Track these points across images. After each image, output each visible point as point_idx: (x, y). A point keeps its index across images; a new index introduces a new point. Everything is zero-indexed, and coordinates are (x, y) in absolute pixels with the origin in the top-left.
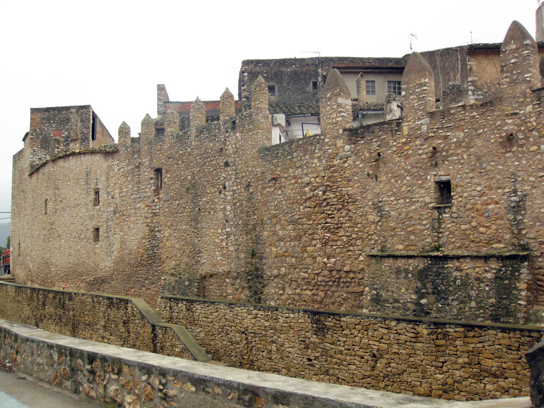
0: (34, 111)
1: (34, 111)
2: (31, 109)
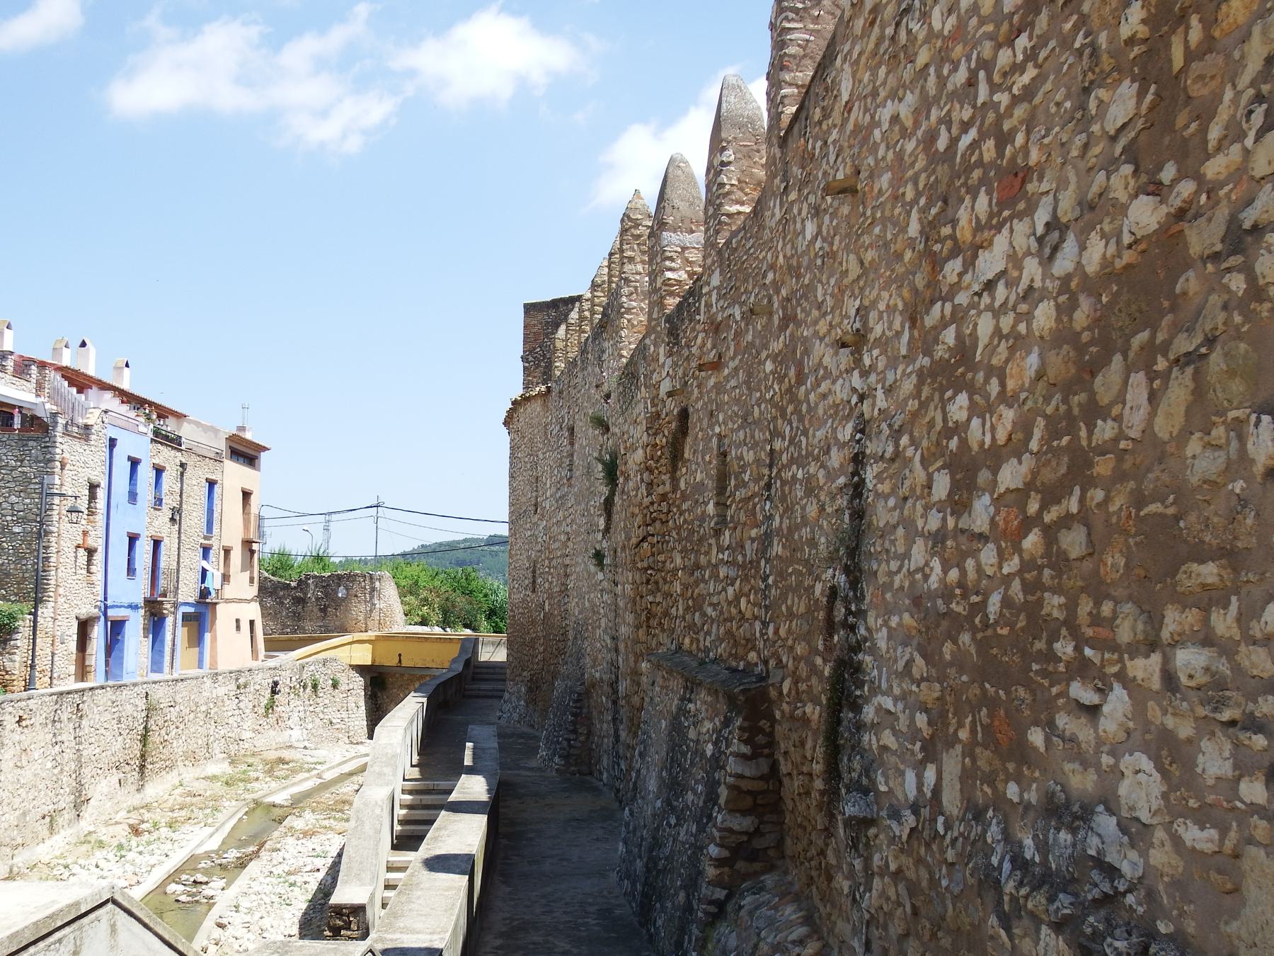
0: (530, 309)
1: (530, 309)
2: (526, 306)
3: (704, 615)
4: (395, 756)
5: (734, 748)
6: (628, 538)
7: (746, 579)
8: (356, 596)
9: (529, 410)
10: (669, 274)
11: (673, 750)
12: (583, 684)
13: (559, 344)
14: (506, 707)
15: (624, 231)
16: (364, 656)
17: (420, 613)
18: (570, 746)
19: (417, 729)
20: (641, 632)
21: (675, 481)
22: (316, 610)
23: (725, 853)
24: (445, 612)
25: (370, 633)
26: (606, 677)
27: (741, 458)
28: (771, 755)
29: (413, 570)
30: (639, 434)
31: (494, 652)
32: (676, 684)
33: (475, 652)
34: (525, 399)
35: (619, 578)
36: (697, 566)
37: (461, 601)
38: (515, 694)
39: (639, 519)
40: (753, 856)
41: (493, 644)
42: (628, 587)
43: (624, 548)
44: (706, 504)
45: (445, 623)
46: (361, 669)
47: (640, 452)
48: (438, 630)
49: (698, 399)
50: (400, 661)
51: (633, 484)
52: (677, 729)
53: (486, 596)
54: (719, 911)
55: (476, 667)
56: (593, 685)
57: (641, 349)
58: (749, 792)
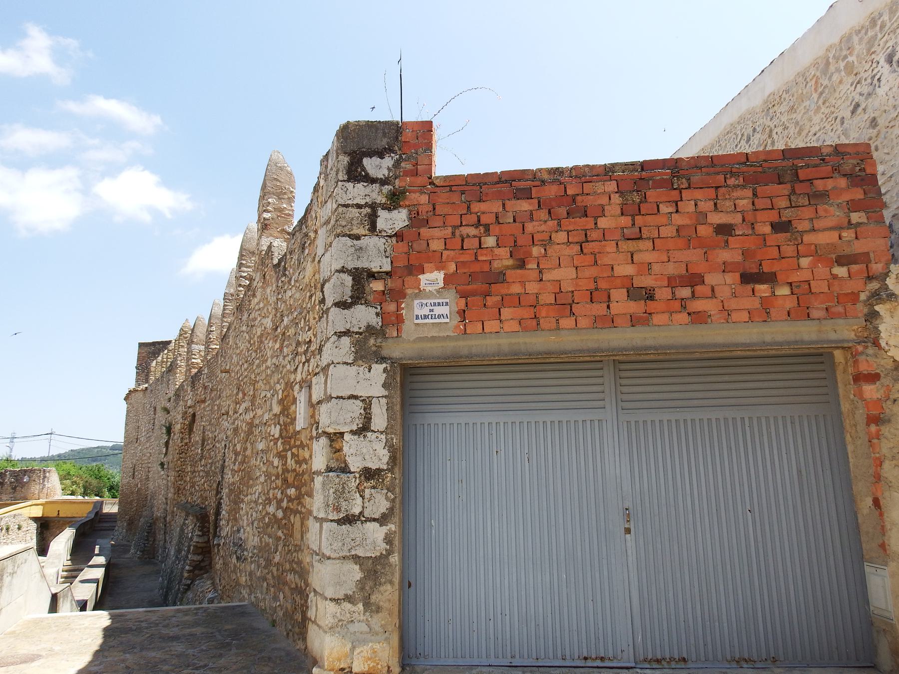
0: (141, 345)
1: (141, 345)
3: (195, 489)
4: (60, 555)
5: (196, 533)
6: (173, 458)
7: (207, 477)
8: (34, 481)
9: (137, 395)
10: (193, 360)
11: (180, 538)
12: (153, 519)
13: (153, 369)
14: (116, 533)
15: (180, 335)
16: (38, 512)
17: (71, 489)
18: (145, 546)
19: (70, 544)
20: (176, 496)
21: (190, 438)
22: (9, 488)
23: (191, 568)
24: (85, 488)
25: (41, 500)
26: (162, 515)
27: (208, 435)
28: (209, 535)
29: (68, 466)
30: (179, 417)
31: (111, 507)
32: (183, 514)
33: (101, 508)
34: (135, 391)
35: (169, 474)
36: (194, 471)
37: (94, 482)
38: (121, 528)
39: (177, 451)
40: (201, 569)
41: (111, 503)
42: (173, 478)
43: (172, 462)
44: (198, 449)
45: (85, 494)
46: (35, 519)
47: (179, 425)
48: (80, 498)
49: (199, 411)
50: (58, 514)
51: (176, 437)
52: (182, 530)
53: (109, 479)
54: (188, 587)
55: (101, 516)
56: (157, 519)
57: (182, 386)
58: (200, 547)
